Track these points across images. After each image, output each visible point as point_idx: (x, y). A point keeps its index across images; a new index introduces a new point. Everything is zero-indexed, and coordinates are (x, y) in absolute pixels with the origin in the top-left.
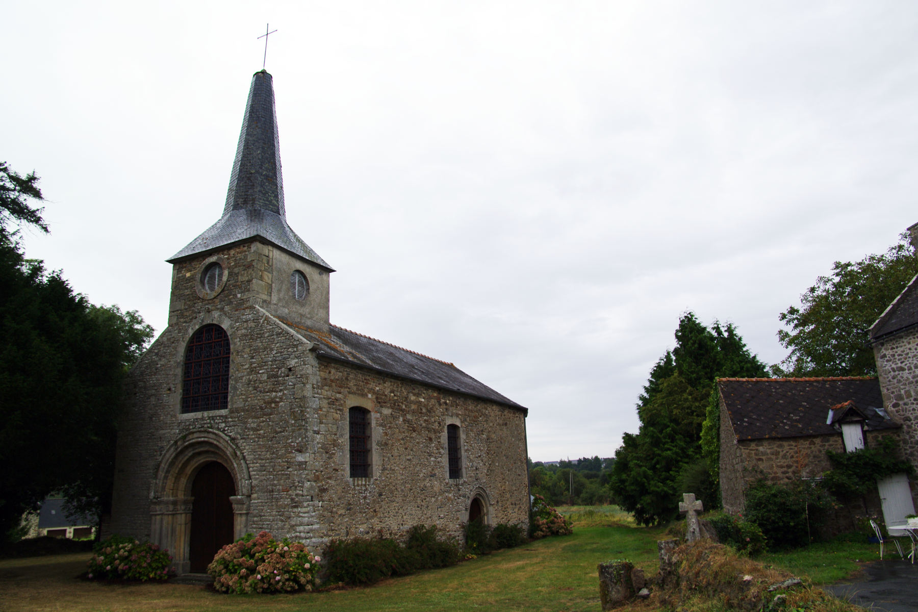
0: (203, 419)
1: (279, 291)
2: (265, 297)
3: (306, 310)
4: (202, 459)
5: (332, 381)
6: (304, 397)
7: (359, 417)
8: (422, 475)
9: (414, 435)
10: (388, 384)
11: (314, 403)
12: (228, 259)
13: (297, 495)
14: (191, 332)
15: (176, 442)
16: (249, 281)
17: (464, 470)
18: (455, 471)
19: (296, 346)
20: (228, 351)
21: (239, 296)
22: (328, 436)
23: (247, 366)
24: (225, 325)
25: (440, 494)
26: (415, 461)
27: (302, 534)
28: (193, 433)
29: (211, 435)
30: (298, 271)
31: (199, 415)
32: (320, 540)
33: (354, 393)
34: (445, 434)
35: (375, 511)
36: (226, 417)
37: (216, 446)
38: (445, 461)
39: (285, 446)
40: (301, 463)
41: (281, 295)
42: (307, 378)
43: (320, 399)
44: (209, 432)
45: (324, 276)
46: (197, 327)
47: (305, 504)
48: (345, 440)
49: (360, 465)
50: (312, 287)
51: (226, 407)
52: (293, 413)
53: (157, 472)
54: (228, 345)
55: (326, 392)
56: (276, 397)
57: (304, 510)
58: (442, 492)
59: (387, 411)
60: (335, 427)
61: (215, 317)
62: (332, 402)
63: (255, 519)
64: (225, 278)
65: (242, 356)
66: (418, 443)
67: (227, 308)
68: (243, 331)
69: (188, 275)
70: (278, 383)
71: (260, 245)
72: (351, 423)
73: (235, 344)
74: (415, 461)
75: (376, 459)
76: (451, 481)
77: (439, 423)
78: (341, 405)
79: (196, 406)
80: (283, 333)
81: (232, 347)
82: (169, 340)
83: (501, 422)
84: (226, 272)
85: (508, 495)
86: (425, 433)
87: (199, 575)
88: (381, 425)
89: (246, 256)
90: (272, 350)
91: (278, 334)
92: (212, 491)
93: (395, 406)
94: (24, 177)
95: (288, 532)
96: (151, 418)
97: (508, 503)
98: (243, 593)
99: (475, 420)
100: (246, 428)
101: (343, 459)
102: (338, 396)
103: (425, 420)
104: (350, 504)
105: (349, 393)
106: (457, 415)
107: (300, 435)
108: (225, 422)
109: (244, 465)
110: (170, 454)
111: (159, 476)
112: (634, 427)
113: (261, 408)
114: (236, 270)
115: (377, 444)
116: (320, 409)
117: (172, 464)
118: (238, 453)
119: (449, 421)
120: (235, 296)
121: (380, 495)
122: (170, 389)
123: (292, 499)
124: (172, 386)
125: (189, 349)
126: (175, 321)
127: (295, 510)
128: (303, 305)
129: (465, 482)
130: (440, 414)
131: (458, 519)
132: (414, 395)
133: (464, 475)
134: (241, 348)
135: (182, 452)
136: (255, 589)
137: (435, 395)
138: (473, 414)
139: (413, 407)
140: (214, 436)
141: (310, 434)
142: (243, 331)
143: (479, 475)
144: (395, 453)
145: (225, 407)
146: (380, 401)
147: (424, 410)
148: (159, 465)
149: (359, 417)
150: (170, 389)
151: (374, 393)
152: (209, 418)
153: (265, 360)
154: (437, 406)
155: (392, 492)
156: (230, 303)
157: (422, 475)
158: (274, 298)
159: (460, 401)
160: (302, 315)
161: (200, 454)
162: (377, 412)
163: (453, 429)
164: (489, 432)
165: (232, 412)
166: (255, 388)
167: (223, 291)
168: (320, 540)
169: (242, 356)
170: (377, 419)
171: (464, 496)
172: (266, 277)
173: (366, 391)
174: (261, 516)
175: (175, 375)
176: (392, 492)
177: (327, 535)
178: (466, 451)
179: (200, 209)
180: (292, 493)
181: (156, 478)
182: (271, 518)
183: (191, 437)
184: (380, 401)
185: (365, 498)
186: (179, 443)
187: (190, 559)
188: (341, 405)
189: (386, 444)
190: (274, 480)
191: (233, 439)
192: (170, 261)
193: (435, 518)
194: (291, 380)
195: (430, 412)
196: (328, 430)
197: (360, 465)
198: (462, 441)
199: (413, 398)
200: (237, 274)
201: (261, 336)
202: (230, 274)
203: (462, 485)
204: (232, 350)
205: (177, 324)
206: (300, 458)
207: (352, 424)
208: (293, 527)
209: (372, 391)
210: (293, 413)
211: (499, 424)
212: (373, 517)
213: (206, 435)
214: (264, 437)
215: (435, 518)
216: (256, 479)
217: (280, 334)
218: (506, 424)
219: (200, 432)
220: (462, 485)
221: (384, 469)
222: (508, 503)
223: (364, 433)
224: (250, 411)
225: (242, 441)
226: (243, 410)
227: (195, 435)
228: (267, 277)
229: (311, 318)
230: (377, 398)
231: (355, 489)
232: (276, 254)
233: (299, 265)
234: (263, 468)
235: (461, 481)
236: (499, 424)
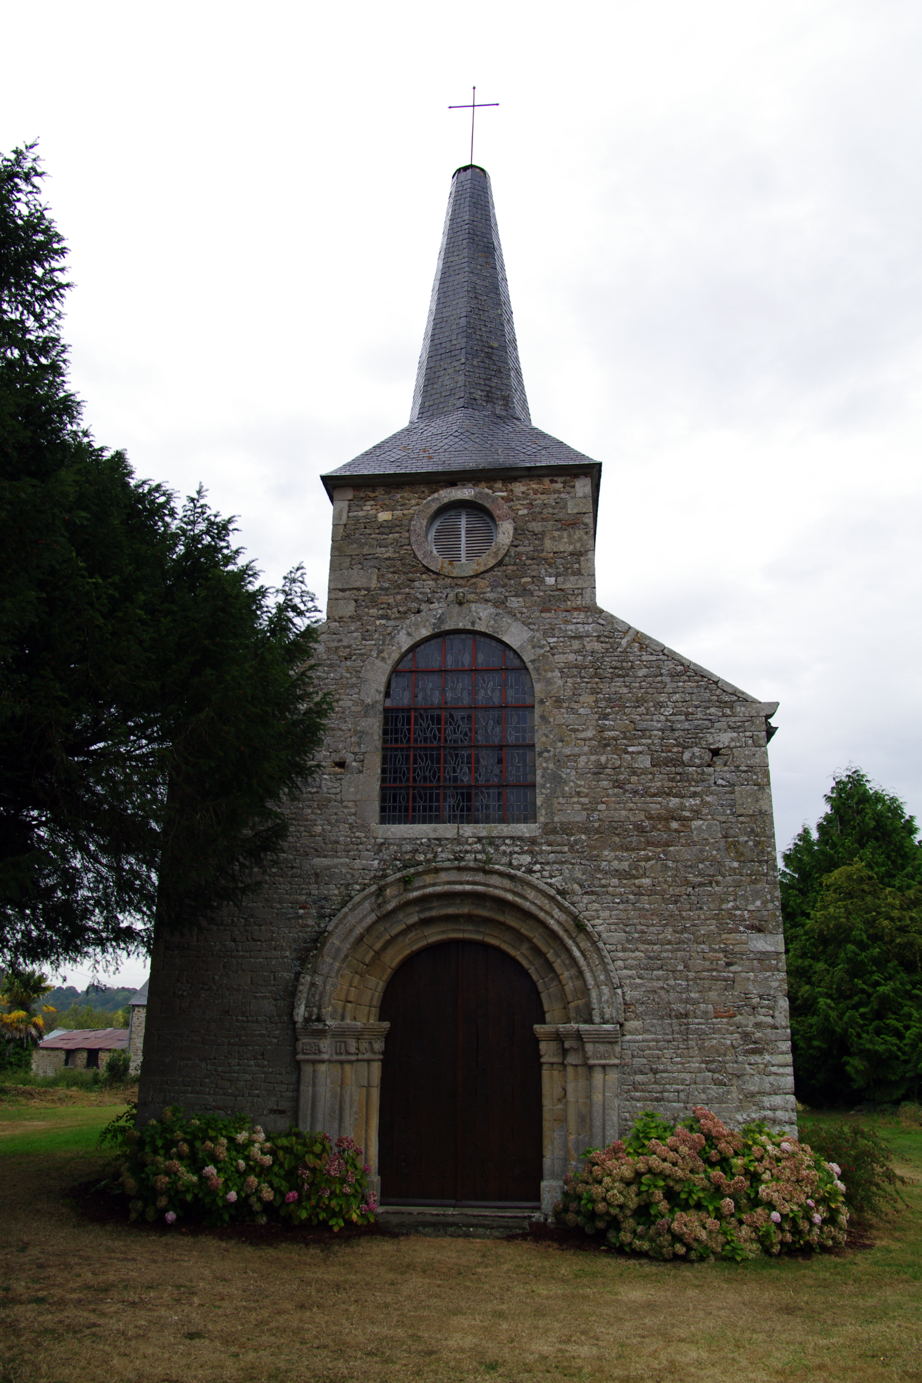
0: (458, 840)
12: (507, 500)
13: (758, 1025)
23: (589, 734)
24: (515, 636)
27: (780, 1114)
31: (447, 830)
36: (533, 841)
39: (716, 917)
52: (733, 846)
56: (682, 808)
63: (639, 1078)
67: (515, 603)
68: (572, 657)
69: (384, 516)
70: (687, 779)
87: (415, 1210)
90: (659, 705)
91: (674, 675)
95: (739, 1109)
98: (729, 1258)
100: (598, 869)
108: (531, 852)
110: (360, 916)
113: (640, 829)
120: (538, 580)
122: (341, 764)
123: (746, 1036)
124: (349, 758)
136: (767, 1251)
140: (507, 883)
142: (572, 657)
145: (529, 816)
150: (341, 764)
152: (480, 840)
153: (643, 725)
156: (524, 592)
165: (549, 830)
166: (618, 784)
169: (574, 711)
174: (655, 1072)
175: (361, 734)
179: (374, 403)
182: (687, 1076)
183: (428, 879)
190: (687, 990)
191: (562, 893)
194: (720, 773)
200: (539, 536)
201: (622, 672)
202: (519, 532)
208: (750, 1096)
210: (733, 846)
213: (480, 877)
214: (652, 893)
216: (635, 987)
217: (679, 674)
225: (586, 899)
226: (586, 831)
227: (443, 876)
234: (653, 963)
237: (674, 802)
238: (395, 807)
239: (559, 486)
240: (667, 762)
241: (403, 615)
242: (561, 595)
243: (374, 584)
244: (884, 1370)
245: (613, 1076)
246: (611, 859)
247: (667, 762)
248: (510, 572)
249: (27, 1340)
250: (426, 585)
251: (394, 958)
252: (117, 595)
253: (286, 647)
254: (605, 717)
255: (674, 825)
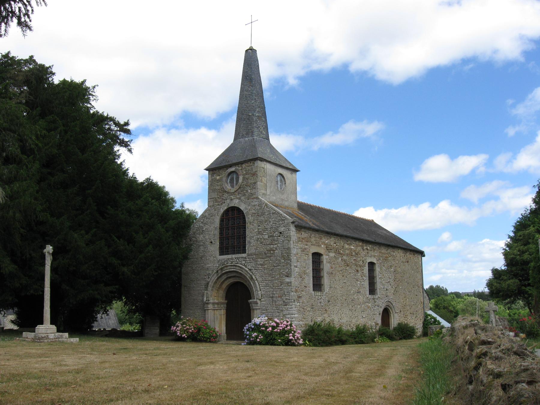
0: (232, 259)
1: (270, 187)
2: (263, 191)
3: (284, 197)
4: (232, 280)
5: (303, 239)
6: (289, 248)
7: (317, 256)
8: (352, 292)
9: (348, 268)
10: (332, 239)
11: (294, 251)
12: (241, 169)
13: (286, 299)
14: (222, 211)
15: (217, 272)
16: (255, 183)
17: (378, 290)
18: (372, 290)
19: (283, 220)
20: (245, 222)
21: (249, 191)
22: (302, 269)
23: (256, 231)
24: (242, 207)
25: (363, 304)
26: (348, 283)
28: (227, 266)
29: (237, 268)
30: (280, 174)
31: (230, 256)
32: (298, 323)
33: (314, 245)
34: (366, 269)
35: (326, 310)
36: (245, 258)
37: (240, 273)
38: (366, 284)
40: (288, 283)
41: (272, 189)
42: (290, 238)
43: (297, 249)
44: (236, 266)
45: (294, 175)
46: (226, 208)
47: (291, 304)
48: (310, 270)
49: (318, 285)
50: (288, 182)
51: (245, 253)
53: (207, 287)
54: (244, 218)
55: (300, 245)
57: (290, 307)
58: (364, 303)
59: (332, 255)
60: (305, 264)
61: (236, 203)
62: (303, 250)
64: (240, 180)
65: (253, 225)
66: (350, 273)
67: (243, 198)
71: (259, 162)
72: (313, 262)
73: (249, 218)
74: (348, 283)
75: (326, 281)
76: (370, 296)
77: (363, 261)
78: (308, 252)
79: (227, 251)
80: (276, 213)
81: (247, 219)
82: (209, 215)
83: (404, 261)
84: (241, 178)
85: (408, 308)
86: (354, 267)
88: (329, 263)
89: (252, 169)
90: (270, 222)
91: (273, 213)
92: (238, 298)
93: (337, 252)
94: (122, 123)
96: (201, 258)
97: (408, 312)
99: (386, 259)
101: (309, 281)
102: (306, 247)
103: (354, 260)
104: (313, 305)
105: (312, 245)
106: (374, 256)
107: (287, 268)
109: (257, 284)
110: (215, 278)
111: (209, 290)
112: (500, 264)
113: (265, 254)
114: (247, 176)
115: (327, 273)
116: (297, 254)
117: (216, 282)
118: (254, 277)
119: (369, 260)
120: (247, 191)
121: (329, 302)
123: (284, 301)
125: (222, 220)
126: (212, 204)
127: (286, 307)
128: (283, 194)
129: (379, 297)
130: (363, 256)
131: (374, 319)
132: (348, 244)
133: (378, 293)
134: (252, 221)
135: (221, 276)
137: (361, 244)
138: (385, 256)
139: (347, 252)
140: (239, 268)
141: (292, 267)
143: (388, 294)
144: (337, 278)
145: (244, 252)
146: (328, 249)
147: (354, 254)
148: (208, 284)
149: (317, 256)
150: (211, 242)
151: (325, 244)
153: (266, 227)
154: (362, 251)
155: (335, 301)
156: (244, 195)
157: (352, 292)
158: (268, 192)
159: (376, 248)
160: (282, 200)
161: (230, 277)
162: (326, 255)
163: (371, 264)
164: (396, 267)
165: (248, 255)
166: (261, 243)
167: (240, 188)
168: (298, 323)
170: (327, 259)
171: (378, 306)
172: (263, 180)
173: (320, 243)
176: (335, 301)
177: (301, 321)
178: (380, 278)
180: (284, 298)
181: (207, 290)
183: (226, 268)
184: (328, 249)
185: (320, 302)
186: (219, 272)
187: (226, 333)
188: (308, 252)
189: (332, 273)
191: (250, 270)
192: (206, 169)
193: (360, 317)
194: (281, 238)
195: (357, 254)
196: (301, 265)
197: (318, 285)
198: (377, 272)
199: (347, 246)
200: (247, 179)
201: (263, 214)
202: (244, 178)
203: (377, 299)
204: (247, 222)
205: (213, 206)
206: (287, 280)
207: (313, 262)
209: (324, 243)
211: (403, 262)
212: (324, 313)
213: (234, 267)
215: (360, 317)
218: (408, 262)
219: (231, 266)
220: (377, 299)
221: (331, 288)
222: (408, 312)
223: (320, 267)
224: (258, 255)
227: (229, 268)
228: (264, 180)
229: (288, 201)
230: (327, 247)
231: (315, 298)
232: (268, 166)
233: (280, 171)
234: (267, 285)
235: (377, 297)
236: (403, 262)
237: (272, 246)
238: (223, 251)
239: (252, 164)
240: (271, 236)
241: (222, 204)
242: (252, 194)
243: (216, 197)
244: (472, 318)
245: (258, 311)
246: (260, 261)
247: (271, 236)
248: (241, 190)
249: (113, 384)
250: (226, 195)
251: (225, 286)
252: (49, 249)
253: (184, 221)
254: (259, 226)
255: (272, 252)
